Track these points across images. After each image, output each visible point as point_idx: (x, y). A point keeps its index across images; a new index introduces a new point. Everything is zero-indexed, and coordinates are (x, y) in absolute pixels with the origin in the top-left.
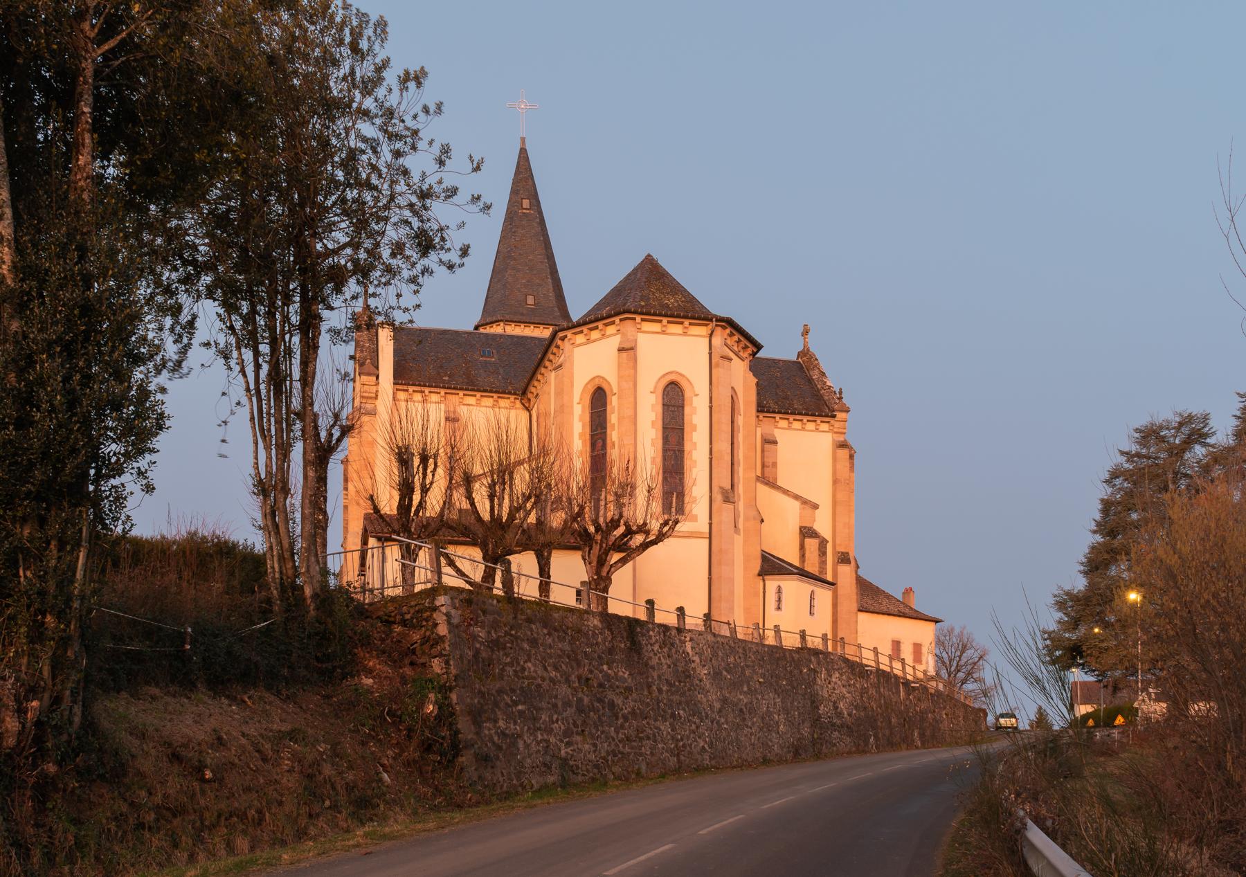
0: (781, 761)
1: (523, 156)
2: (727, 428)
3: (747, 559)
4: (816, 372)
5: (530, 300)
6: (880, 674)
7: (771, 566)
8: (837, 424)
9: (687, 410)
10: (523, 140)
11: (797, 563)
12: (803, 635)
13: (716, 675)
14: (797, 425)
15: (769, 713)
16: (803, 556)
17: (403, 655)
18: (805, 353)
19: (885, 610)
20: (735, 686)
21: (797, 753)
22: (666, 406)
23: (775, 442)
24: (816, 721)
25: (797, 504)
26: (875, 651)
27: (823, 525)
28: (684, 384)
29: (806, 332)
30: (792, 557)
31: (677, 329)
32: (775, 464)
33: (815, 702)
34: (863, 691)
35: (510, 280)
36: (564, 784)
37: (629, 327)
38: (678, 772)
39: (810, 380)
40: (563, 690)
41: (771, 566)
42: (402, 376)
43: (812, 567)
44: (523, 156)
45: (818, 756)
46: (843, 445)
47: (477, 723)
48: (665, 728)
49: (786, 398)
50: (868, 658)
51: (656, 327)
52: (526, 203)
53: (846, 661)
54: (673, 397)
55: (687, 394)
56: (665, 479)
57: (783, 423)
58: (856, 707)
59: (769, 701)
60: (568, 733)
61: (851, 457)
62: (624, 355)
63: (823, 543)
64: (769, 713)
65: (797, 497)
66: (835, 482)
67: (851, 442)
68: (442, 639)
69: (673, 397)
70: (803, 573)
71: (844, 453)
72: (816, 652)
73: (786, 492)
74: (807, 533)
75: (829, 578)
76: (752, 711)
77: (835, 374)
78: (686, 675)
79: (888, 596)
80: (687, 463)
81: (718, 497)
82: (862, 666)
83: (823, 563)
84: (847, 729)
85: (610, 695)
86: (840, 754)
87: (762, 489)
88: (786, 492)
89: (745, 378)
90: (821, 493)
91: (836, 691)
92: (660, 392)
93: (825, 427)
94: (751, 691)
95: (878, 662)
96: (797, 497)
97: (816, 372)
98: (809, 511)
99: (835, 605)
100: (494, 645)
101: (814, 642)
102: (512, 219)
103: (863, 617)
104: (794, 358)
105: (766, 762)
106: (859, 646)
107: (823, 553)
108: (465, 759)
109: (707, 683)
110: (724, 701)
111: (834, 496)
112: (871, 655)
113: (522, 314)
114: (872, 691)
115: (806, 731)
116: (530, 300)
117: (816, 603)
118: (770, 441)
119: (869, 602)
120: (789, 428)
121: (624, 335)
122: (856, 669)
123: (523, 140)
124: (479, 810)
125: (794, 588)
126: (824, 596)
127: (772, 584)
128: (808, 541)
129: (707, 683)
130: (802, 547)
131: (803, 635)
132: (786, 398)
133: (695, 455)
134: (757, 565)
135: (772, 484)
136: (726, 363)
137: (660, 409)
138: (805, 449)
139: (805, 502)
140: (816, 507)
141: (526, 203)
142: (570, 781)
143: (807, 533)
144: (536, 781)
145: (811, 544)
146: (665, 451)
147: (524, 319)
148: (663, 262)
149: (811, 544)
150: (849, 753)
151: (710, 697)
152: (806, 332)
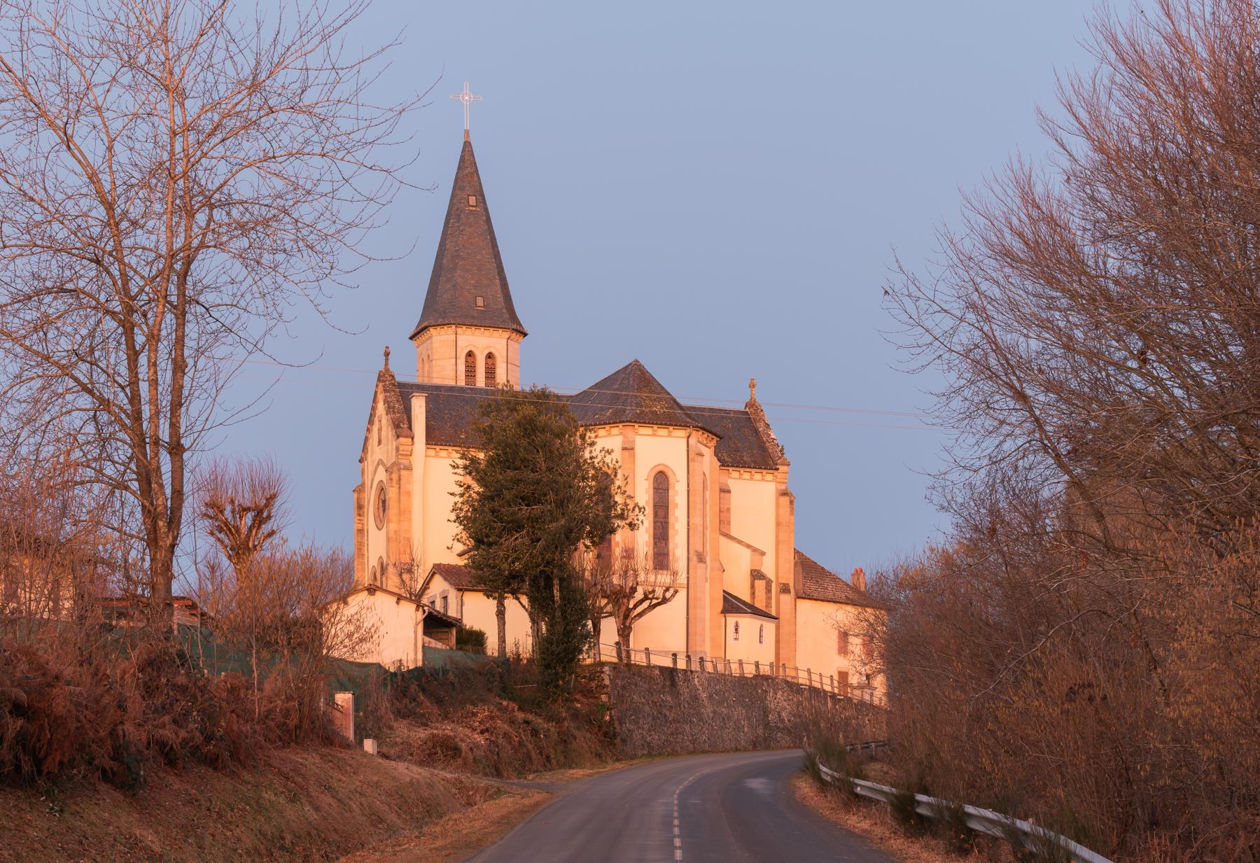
0: (746, 750)
2: (700, 506)
3: (712, 600)
4: (762, 424)
5: (480, 301)
6: (813, 690)
7: (731, 605)
8: (779, 476)
9: (671, 493)
10: (467, 133)
11: (747, 599)
12: (757, 665)
13: (710, 697)
14: (747, 476)
15: (739, 720)
16: (753, 594)
17: (588, 693)
18: (751, 404)
19: (830, 596)
20: (720, 703)
21: (755, 745)
22: (656, 489)
23: (729, 492)
24: (767, 725)
25: (748, 551)
26: (809, 671)
27: (768, 568)
28: (669, 473)
29: (752, 386)
30: (745, 596)
31: (663, 432)
32: (728, 510)
33: (766, 712)
34: (799, 703)
35: (459, 280)
37: (629, 431)
39: (756, 432)
40: (647, 708)
41: (731, 605)
42: (433, 438)
43: (760, 604)
45: (767, 748)
46: (785, 494)
47: (621, 724)
48: (687, 728)
49: (737, 450)
51: (648, 431)
52: (472, 200)
53: (787, 682)
54: (661, 482)
55: (671, 480)
56: (655, 543)
57: (735, 474)
58: (794, 716)
59: (739, 712)
60: (649, 730)
61: (791, 502)
62: (627, 453)
63: (769, 582)
64: (739, 720)
65: (748, 546)
66: (778, 524)
67: (791, 490)
68: (605, 686)
69: (661, 482)
70: (756, 612)
71: (786, 500)
72: (766, 678)
73: (740, 542)
74: (756, 575)
75: (774, 613)
76: (729, 718)
77: (778, 432)
78: (695, 698)
79: (835, 579)
80: (671, 532)
81: (694, 559)
82: (798, 685)
84: (789, 732)
85: (664, 711)
86: (782, 748)
88: (740, 542)
89: (711, 463)
90: (766, 542)
91: (780, 704)
92: (652, 479)
93: (769, 477)
94: (729, 707)
95: (810, 680)
96: (748, 546)
97: (762, 424)
98: (757, 557)
99: (778, 635)
100: (624, 687)
101: (765, 670)
102: (455, 215)
104: (741, 408)
105: (737, 750)
106: (796, 669)
107: (769, 591)
108: (618, 740)
109: (706, 702)
110: (715, 712)
111: (777, 536)
112: (805, 675)
113: (473, 317)
114: (806, 704)
115: (760, 731)
116: (480, 301)
117: (764, 633)
118: (725, 491)
119: (812, 587)
120: (740, 478)
121: (625, 437)
122: (794, 687)
123: (467, 133)
124: (644, 759)
125: (748, 623)
126: (770, 627)
127: (731, 619)
128: (757, 582)
129: (706, 702)
130: (753, 586)
131: (757, 665)
132: (737, 450)
133: (677, 526)
134: (720, 605)
136: (699, 458)
137: (651, 491)
138: (754, 495)
139: (755, 550)
140: (763, 554)
141: (472, 200)
142: (653, 752)
143: (756, 575)
144: (640, 753)
145: (760, 584)
146: (655, 522)
147: (476, 322)
149: (760, 584)
150: (789, 748)
151: (708, 710)
152: (752, 386)
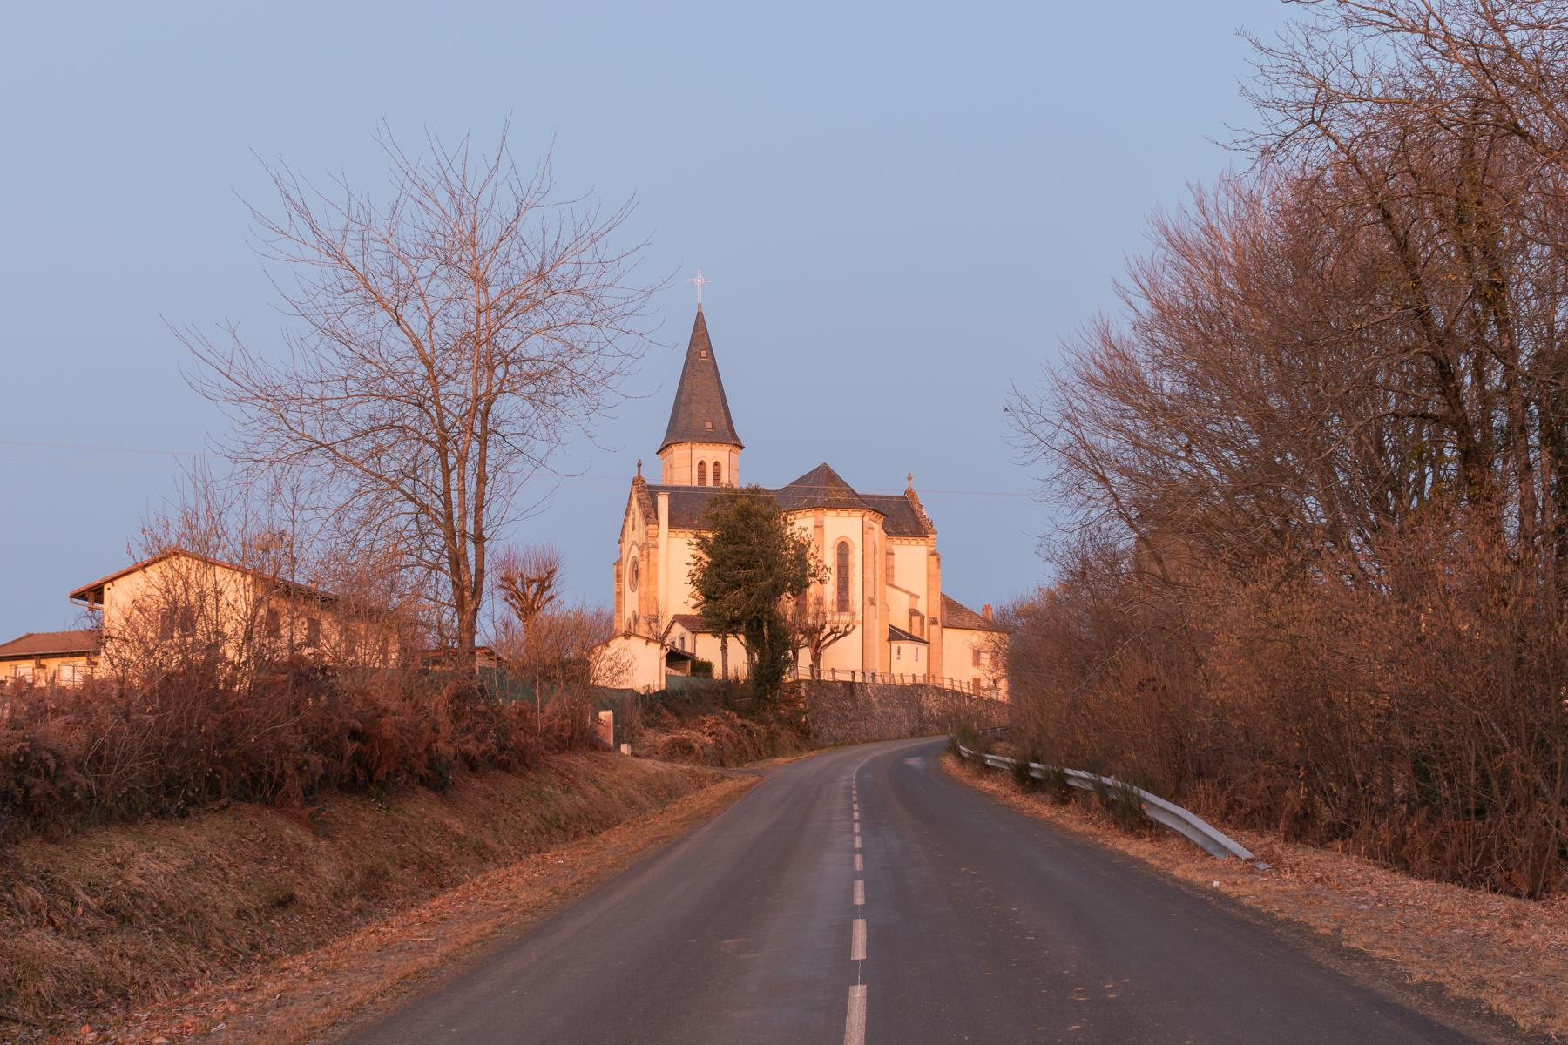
1: (700, 314)
5: (709, 425)
6: (955, 692)
7: (895, 635)
10: (700, 306)
18: (909, 491)
24: (921, 719)
29: (910, 478)
31: (844, 513)
33: (920, 710)
36: (835, 745)
37: (819, 514)
38: (867, 742)
39: (913, 511)
41: (895, 635)
42: (673, 524)
43: (916, 633)
44: (700, 314)
45: (922, 735)
46: (933, 554)
50: (947, 685)
52: (704, 353)
54: (843, 549)
59: (901, 711)
63: (922, 617)
66: (929, 576)
69: (843, 549)
71: (934, 558)
72: (921, 686)
74: (913, 612)
78: (869, 702)
79: (970, 613)
83: (922, 629)
87: (888, 588)
91: (931, 703)
101: (920, 680)
102: (691, 364)
103: (948, 633)
107: (922, 623)
116: (709, 425)
118: (890, 553)
122: (941, 691)
125: (907, 647)
126: (923, 649)
127: (895, 645)
135: (892, 586)
138: (911, 557)
139: (912, 595)
141: (704, 353)
142: (837, 743)
143: (913, 612)
145: (916, 619)
148: (834, 468)
149: (916, 619)
151: (878, 711)
152: (910, 478)
